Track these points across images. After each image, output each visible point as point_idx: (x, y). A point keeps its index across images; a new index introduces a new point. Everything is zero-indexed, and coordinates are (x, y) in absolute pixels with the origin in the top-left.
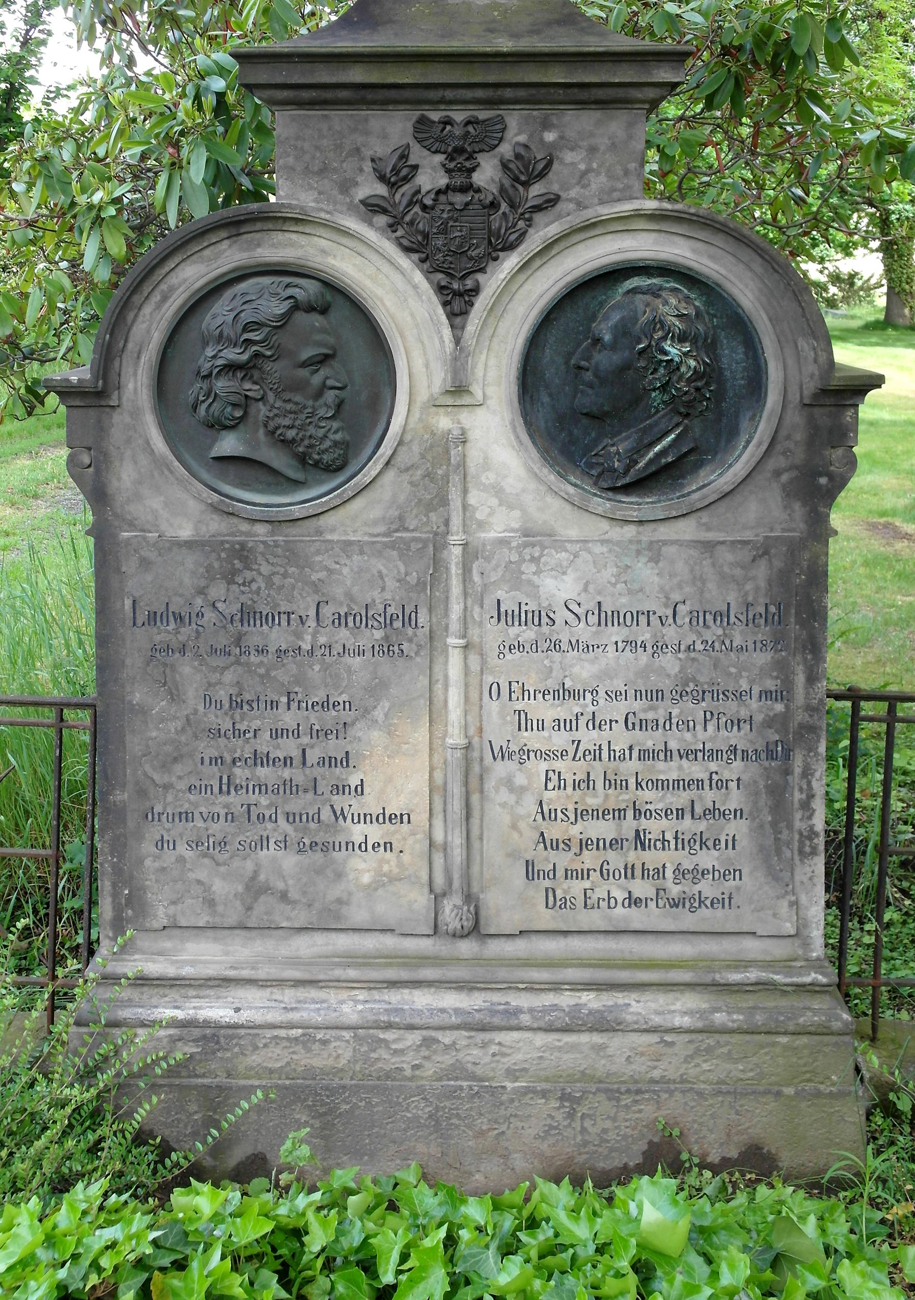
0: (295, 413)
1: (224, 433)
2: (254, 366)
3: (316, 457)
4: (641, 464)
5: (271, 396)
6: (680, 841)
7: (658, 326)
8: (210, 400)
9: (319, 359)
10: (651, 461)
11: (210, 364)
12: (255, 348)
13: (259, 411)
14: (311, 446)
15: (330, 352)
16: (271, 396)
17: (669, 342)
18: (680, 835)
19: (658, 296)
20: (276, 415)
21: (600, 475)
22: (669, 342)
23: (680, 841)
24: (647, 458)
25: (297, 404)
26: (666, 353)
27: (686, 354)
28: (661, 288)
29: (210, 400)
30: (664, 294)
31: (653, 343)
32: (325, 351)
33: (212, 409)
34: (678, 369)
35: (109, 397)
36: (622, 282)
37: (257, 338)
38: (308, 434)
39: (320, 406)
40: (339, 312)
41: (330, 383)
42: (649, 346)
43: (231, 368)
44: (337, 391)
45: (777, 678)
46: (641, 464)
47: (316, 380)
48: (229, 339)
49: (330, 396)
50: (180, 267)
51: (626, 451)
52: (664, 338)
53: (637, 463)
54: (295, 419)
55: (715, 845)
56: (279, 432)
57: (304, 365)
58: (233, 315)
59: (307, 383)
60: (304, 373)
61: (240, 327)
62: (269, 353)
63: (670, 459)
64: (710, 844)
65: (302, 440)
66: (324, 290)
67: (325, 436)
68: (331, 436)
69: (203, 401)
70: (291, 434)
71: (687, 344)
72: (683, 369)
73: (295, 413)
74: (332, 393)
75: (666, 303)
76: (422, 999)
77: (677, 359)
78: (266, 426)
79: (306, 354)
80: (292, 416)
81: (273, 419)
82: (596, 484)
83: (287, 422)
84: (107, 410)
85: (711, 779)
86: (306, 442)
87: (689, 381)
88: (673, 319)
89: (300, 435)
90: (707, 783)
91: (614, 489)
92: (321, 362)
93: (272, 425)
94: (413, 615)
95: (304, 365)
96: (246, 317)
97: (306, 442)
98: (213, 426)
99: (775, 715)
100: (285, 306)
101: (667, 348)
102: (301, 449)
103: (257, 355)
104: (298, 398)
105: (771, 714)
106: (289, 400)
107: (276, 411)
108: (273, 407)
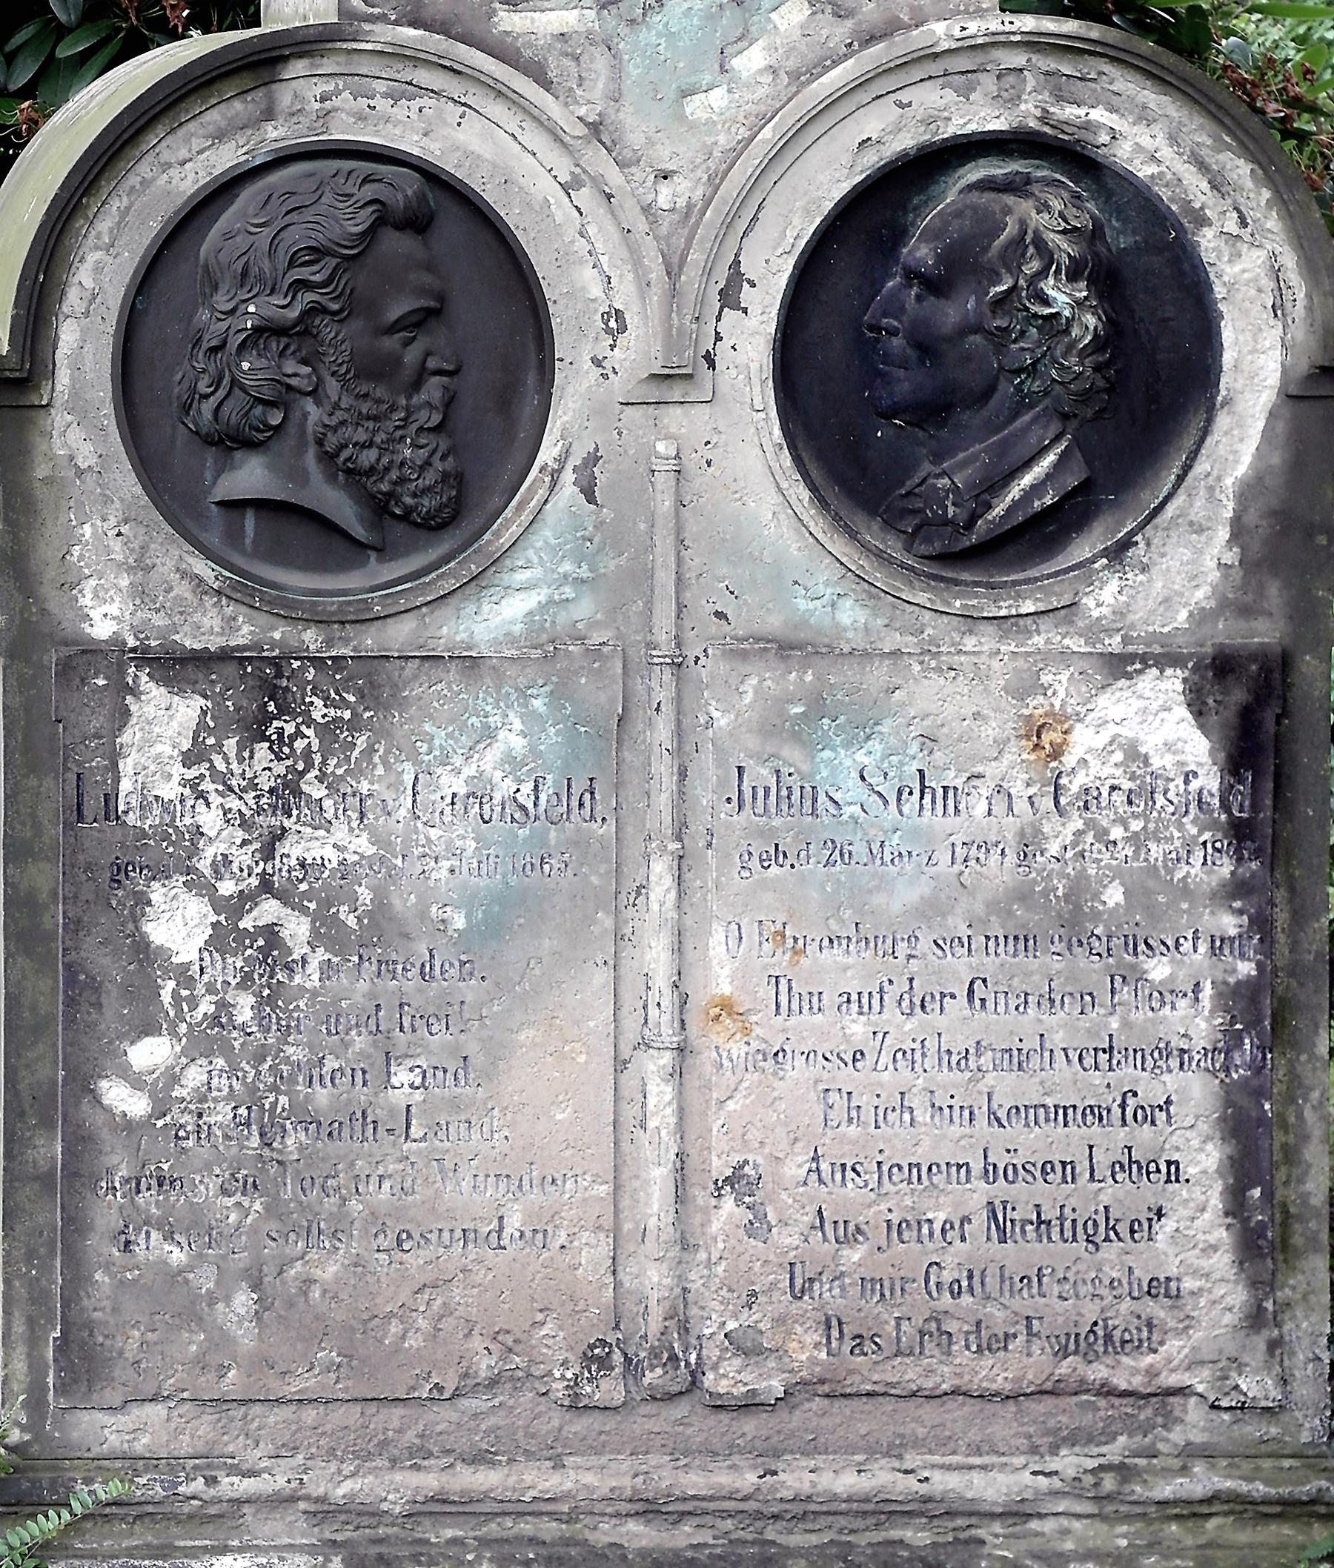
0: (375, 418)
1: (238, 455)
2: (306, 332)
3: (408, 500)
4: (998, 511)
5: (332, 386)
6: (1068, 1224)
7: (1031, 250)
8: (221, 393)
9: (414, 319)
10: (1015, 505)
11: (225, 325)
12: (310, 296)
13: (305, 415)
14: (402, 481)
15: (432, 304)
16: (332, 386)
17: (1051, 281)
18: (1067, 1211)
19: (1029, 195)
20: (343, 423)
21: (918, 529)
22: (1051, 281)
23: (1068, 1224)
24: (1009, 499)
25: (379, 401)
26: (1046, 301)
27: (1079, 303)
28: (1028, 180)
29: (221, 393)
30: (1035, 188)
31: (1022, 282)
32: (423, 303)
33: (226, 410)
34: (1067, 332)
35: (37, 388)
36: (954, 171)
37: (317, 278)
38: (398, 459)
39: (419, 408)
40: (451, 226)
41: (432, 363)
42: (1014, 288)
43: (265, 331)
44: (445, 379)
45: (1240, 912)
46: (998, 511)
47: (411, 356)
48: (260, 279)
49: (433, 389)
50: (488, 91)
51: (970, 485)
52: (1043, 273)
53: (989, 507)
54: (375, 432)
55: (1132, 1232)
56: (345, 454)
57: (392, 329)
58: (267, 233)
59: (397, 362)
60: (391, 343)
61: (283, 260)
62: (335, 307)
63: (1048, 501)
64: (1123, 1229)
65: (387, 469)
66: (427, 189)
67: (427, 464)
68: (439, 465)
69: (207, 396)
70: (367, 458)
71: (1083, 284)
72: (1075, 332)
73: (375, 418)
74: (435, 380)
75: (1046, 207)
76: (847, 1482)
77: (1067, 313)
78: (320, 443)
79: (395, 312)
80: (371, 424)
81: (335, 429)
82: (908, 548)
83: (361, 436)
84: (12, 413)
85: (1123, 1106)
86: (394, 475)
87: (1083, 354)
88: (1057, 238)
89: (385, 460)
90: (1116, 1111)
91: (944, 558)
92: (418, 325)
93: (332, 441)
94: (587, 796)
95: (392, 329)
96: (297, 237)
97: (394, 475)
98: (221, 441)
99: (1239, 983)
100: (366, 217)
101: (1051, 292)
102: (384, 487)
103: (313, 311)
104: (380, 392)
105: (1232, 980)
106: (366, 395)
107: (339, 415)
108: (336, 406)
